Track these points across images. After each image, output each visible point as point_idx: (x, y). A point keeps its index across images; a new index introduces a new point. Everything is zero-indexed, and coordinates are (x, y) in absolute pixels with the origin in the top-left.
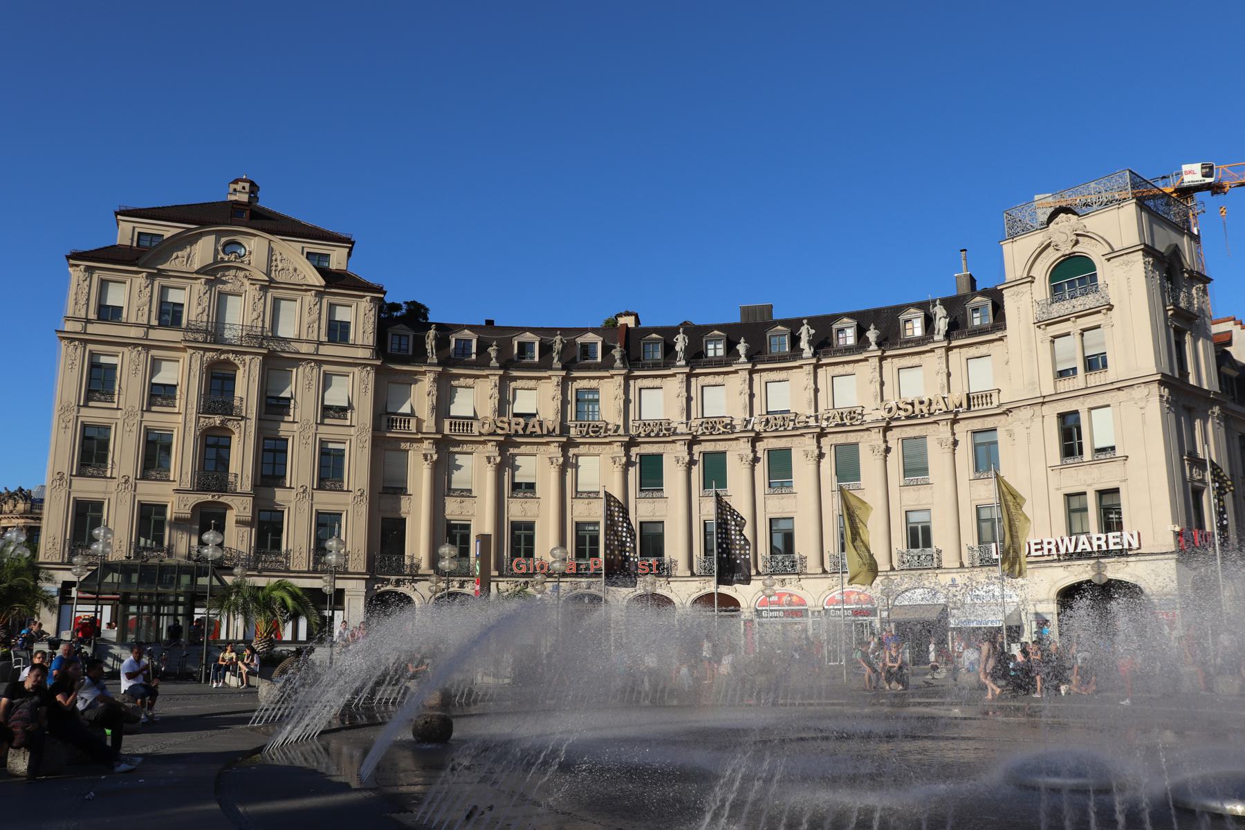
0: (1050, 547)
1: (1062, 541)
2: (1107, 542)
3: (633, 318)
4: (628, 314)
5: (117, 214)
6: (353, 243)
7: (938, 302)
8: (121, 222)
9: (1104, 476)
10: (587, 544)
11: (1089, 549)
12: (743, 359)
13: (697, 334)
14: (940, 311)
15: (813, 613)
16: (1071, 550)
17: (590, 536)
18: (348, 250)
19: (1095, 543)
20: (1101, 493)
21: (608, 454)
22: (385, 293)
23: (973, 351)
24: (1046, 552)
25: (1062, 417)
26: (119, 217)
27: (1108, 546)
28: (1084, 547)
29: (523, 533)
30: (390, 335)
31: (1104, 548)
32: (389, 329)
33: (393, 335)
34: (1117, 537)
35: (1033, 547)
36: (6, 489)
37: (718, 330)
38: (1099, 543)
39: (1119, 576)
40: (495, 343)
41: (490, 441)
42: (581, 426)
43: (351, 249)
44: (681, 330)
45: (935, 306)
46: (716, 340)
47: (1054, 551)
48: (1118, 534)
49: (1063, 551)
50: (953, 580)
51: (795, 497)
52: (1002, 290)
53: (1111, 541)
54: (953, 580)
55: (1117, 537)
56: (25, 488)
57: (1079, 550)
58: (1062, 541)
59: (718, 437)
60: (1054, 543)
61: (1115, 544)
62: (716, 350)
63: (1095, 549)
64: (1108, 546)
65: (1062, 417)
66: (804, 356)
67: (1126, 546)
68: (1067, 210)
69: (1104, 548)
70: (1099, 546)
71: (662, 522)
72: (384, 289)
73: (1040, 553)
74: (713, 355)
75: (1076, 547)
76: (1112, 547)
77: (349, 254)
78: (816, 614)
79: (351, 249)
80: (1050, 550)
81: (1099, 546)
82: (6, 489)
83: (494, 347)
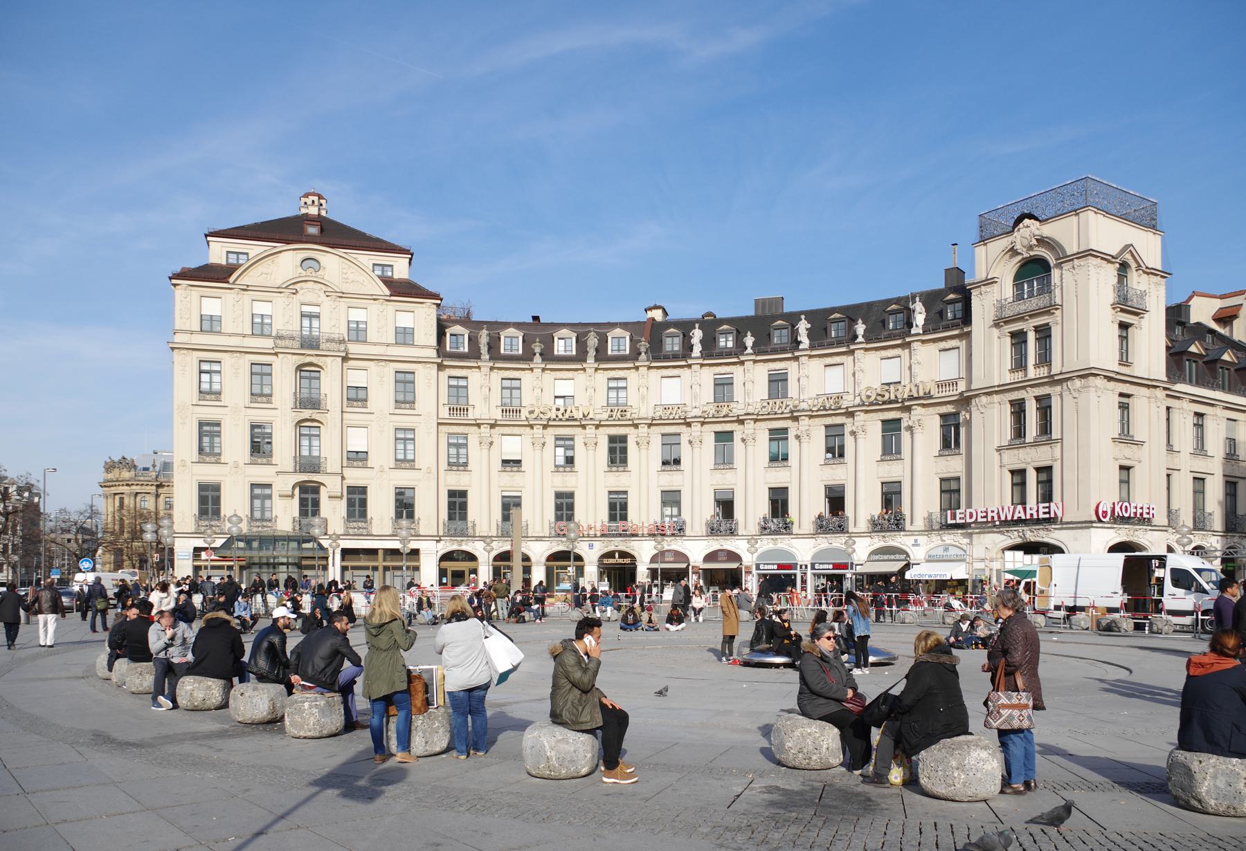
0: (993, 514)
1: (1003, 509)
2: (1038, 511)
3: (661, 311)
4: (656, 307)
5: (206, 236)
6: (412, 255)
7: (917, 299)
8: (211, 243)
9: (1042, 456)
10: (357, 505)
11: (1023, 517)
12: (749, 350)
13: (711, 325)
14: (918, 307)
15: (801, 566)
16: (1009, 518)
17: (212, 497)
18: (408, 260)
19: (1029, 512)
20: (1039, 470)
21: (528, 434)
22: (441, 300)
23: (559, 374)
24: (989, 519)
25: (612, 439)
26: (209, 238)
27: (1038, 515)
28: (1019, 515)
29: (210, 494)
30: (448, 335)
31: (1035, 517)
32: (447, 330)
33: (451, 335)
34: (1046, 507)
35: (980, 515)
36: (110, 458)
37: (838, 312)
38: (993, 514)
39: (1046, 540)
40: (538, 340)
41: (692, 418)
42: (612, 411)
43: (411, 259)
44: (697, 325)
45: (914, 302)
46: (726, 333)
47: (996, 519)
48: (1047, 505)
49: (1003, 518)
50: (916, 541)
51: (469, 474)
52: (971, 289)
53: (1041, 510)
54: (916, 541)
55: (1046, 507)
56: (129, 458)
57: (1015, 518)
58: (1003, 509)
59: (674, 421)
60: (996, 512)
61: (1045, 513)
62: (726, 342)
63: (1028, 517)
64: (1038, 515)
65: (612, 439)
66: (693, 355)
67: (1052, 515)
68: (1031, 216)
69: (1035, 517)
70: (1032, 515)
71: (680, 491)
72: (441, 296)
73: (985, 520)
74: (670, 349)
75: (1013, 517)
76: (1042, 516)
77: (410, 263)
78: (804, 567)
79: (411, 259)
80: (993, 517)
81: (1032, 515)
82: (110, 458)
83: (538, 344)
